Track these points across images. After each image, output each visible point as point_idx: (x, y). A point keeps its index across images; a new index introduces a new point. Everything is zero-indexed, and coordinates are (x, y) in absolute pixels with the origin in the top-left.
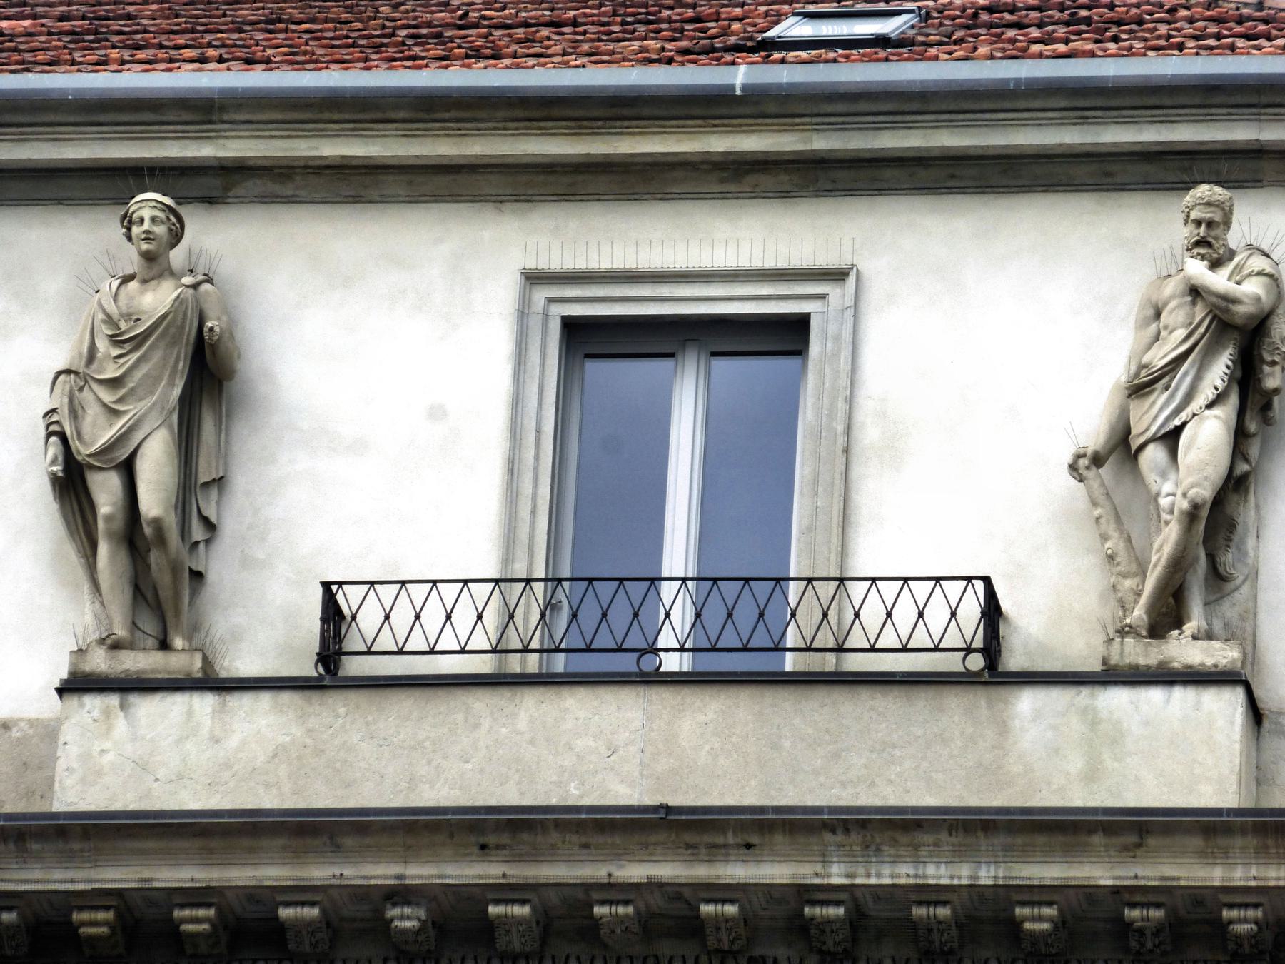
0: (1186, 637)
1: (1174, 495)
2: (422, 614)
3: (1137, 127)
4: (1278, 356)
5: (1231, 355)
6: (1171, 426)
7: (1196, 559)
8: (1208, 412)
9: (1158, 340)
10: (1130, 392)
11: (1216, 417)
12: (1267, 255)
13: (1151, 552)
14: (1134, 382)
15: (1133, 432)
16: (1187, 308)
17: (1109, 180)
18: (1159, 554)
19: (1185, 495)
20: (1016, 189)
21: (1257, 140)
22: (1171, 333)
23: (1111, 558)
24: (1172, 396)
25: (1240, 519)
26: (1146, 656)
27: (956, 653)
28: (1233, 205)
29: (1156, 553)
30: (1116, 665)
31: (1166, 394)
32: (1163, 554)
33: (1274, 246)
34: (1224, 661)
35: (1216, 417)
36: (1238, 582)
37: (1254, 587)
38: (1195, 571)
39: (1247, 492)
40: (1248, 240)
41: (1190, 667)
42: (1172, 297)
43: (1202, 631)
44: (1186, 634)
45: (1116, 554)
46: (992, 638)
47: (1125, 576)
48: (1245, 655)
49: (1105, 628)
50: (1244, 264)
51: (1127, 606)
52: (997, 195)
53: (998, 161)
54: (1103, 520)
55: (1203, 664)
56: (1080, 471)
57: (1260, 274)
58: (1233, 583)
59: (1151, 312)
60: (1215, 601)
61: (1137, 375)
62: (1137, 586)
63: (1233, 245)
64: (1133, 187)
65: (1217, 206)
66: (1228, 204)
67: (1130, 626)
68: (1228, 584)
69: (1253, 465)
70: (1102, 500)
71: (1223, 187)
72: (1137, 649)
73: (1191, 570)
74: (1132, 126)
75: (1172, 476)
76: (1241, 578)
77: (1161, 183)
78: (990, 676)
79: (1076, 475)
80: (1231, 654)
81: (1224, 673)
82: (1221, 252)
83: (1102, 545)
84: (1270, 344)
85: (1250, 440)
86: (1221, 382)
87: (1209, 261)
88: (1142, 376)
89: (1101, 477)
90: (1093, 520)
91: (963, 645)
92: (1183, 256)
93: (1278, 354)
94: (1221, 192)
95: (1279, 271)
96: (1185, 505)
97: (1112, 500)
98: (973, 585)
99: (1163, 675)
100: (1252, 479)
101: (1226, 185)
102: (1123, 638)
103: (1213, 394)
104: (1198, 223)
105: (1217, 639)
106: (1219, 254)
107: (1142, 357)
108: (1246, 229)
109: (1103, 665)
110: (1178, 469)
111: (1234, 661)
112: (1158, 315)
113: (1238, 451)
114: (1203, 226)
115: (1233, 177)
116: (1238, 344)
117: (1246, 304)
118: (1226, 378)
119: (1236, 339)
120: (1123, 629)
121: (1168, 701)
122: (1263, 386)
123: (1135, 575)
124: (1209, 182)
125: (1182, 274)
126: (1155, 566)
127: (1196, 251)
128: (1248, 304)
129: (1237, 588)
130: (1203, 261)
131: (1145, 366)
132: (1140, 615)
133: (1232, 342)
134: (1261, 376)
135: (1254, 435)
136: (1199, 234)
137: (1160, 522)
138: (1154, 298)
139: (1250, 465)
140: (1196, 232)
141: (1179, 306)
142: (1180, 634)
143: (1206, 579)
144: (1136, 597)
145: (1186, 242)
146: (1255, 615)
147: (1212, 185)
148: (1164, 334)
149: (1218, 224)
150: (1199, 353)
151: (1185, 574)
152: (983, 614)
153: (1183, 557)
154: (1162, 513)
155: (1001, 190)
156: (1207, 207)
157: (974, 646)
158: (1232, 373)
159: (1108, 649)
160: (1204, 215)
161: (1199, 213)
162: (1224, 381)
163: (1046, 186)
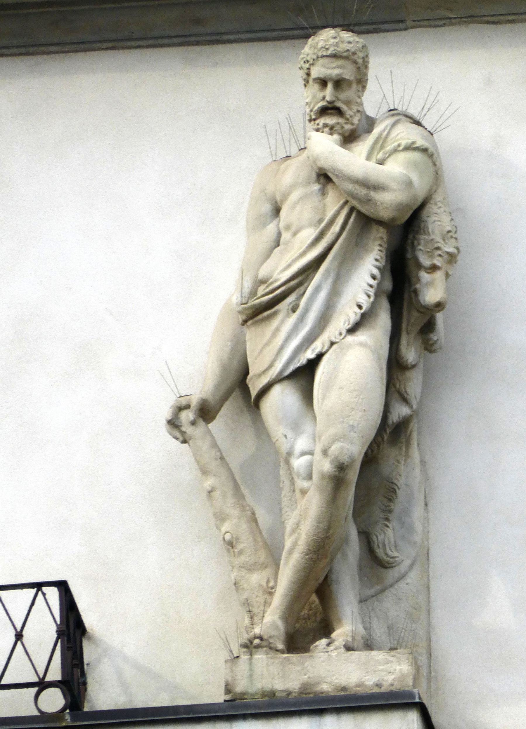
0: (336, 649)
1: (311, 453)
2: (24, 633)
4: (440, 259)
5: (377, 260)
7: (346, 540)
8: (350, 339)
9: (278, 245)
10: (244, 317)
11: (362, 345)
12: (418, 123)
13: (283, 534)
14: (251, 304)
16: (315, 200)
19: (325, 453)
20: (73, 47)
22: (295, 234)
23: (231, 544)
25: (401, 482)
27: (25, 690)
28: (367, 56)
29: (289, 538)
30: (243, 694)
31: (294, 317)
32: (300, 534)
33: (426, 109)
34: (391, 678)
35: (362, 345)
37: (426, 572)
38: (345, 554)
39: (408, 443)
40: (391, 103)
41: (344, 689)
42: (293, 187)
43: (358, 638)
44: (337, 643)
45: (237, 539)
46: (73, 666)
47: (251, 568)
48: (417, 668)
49: (227, 643)
50: (387, 137)
51: (255, 610)
52: (45, 57)
53: (45, 10)
54: (217, 494)
55: (361, 685)
57: (409, 148)
58: (396, 569)
59: (267, 208)
60: (373, 596)
61: (253, 293)
62: (268, 581)
63: (371, 112)
64: (232, 37)
65: (347, 58)
66: (361, 55)
67: (261, 638)
68: (391, 571)
69: (415, 407)
70: (214, 465)
71: (353, 32)
73: (339, 555)
75: (308, 428)
76: (407, 563)
77: (268, 31)
78: (73, 719)
79: (178, 435)
80: (398, 668)
82: (356, 121)
83: (218, 528)
84: (427, 242)
86: (366, 297)
87: (340, 134)
88: (259, 294)
89: (211, 435)
90: (205, 494)
91: (34, 679)
92: (305, 128)
93: (440, 255)
94: (351, 39)
95: (434, 145)
97: (227, 465)
98: (44, 594)
99: (308, 702)
100: (414, 426)
101: (356, 28)
102: (251, 654)
103: (356, 313)
104: (323, 83)
105: (379, 649)
106: (353, 124)
107: (258, 269)
108: (387, 88)
109: (225, 694)
110: (315, 418)
111: (403, 677)
112: (277, 211)
113: (393, 389)
114: (330, 86)
115: (365, 18)
116: (385, 246)
118: (372, 292)
119: (382, 238)
120: (251, 643)
122: (421, 299)
123: (263, 566)
124: (334, 27)
125: (306, 153)
126: (291, 552)
127: (322, 121)
128: (395, 190)
129: (402, 577)
130: (331, 134)
131: (263, 282)
132: (274, 622)
134: (417, 286)
135: (414, 366)
136: (324, 98)
137: (294, 491)
138: (270, 189)
139: (411, 407)
141: (304, 198)
142: (328, 645)
143: (360, 567)
144: (267, 596)
145: (308, 110)
146: (429, 612)
147: (338, 29)
148: (286, 236)
149: (349, 83)
150: (334, 259)
151: (332, 560)
152: (60, 634)
153: (327, 537)
154: (296, 479)
155: (52, 49)
156: (332, 60)
157: (48, 679)
158: (379, 284)
159: (232, 671)
161: (323, 70)
162: (369, 296)
163: (114, 41)
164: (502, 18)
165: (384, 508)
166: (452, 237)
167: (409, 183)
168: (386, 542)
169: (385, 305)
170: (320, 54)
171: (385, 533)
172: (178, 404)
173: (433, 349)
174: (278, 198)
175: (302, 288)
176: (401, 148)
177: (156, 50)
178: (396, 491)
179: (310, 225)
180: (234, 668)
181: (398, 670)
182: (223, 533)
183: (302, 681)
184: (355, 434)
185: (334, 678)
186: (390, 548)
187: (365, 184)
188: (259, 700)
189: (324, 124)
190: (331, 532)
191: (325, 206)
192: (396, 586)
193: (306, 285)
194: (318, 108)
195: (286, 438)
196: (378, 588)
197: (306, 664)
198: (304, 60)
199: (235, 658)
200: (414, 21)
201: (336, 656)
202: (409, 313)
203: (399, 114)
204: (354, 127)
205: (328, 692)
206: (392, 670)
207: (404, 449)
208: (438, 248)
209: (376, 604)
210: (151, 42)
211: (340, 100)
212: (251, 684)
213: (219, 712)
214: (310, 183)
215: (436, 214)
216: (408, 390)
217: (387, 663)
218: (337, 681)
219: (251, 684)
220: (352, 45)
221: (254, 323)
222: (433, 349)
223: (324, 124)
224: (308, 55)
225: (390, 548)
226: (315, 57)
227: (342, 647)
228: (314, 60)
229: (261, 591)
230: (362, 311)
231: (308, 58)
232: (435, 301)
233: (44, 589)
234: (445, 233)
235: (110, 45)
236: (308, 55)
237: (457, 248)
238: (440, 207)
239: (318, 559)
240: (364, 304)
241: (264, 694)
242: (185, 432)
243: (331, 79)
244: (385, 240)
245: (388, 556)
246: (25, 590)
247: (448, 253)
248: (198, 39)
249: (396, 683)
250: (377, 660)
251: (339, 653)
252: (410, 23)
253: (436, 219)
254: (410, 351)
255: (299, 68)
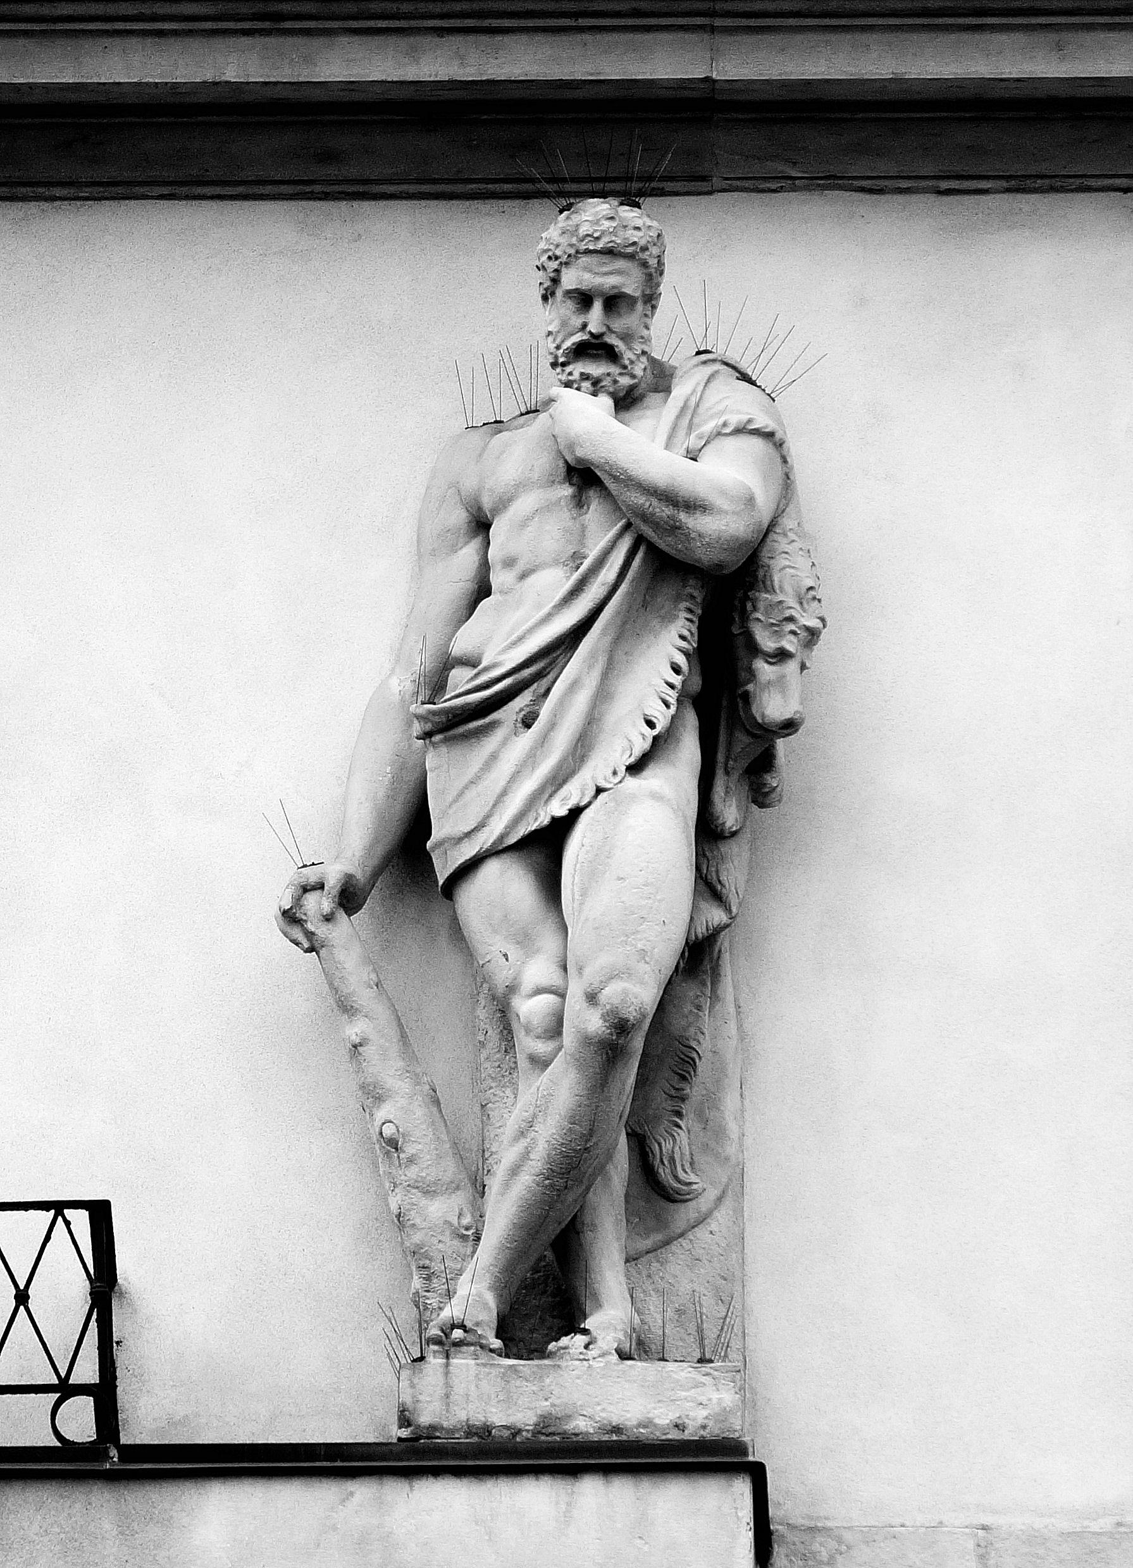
0: (603, 1355)
2: (30, 1292)
3: (403, 42)
4: (792, 637)
5: (683, 638)
6: (541, 818)
8: (632, 782)
11: (656, 797)
15: (437, 833)
17: (332, 171)
18: (523, 1143)
20: (96, 190)
21: (707, 79)
22: (523, 576)
24: (544, 740)
25: (704, 1046)
26: (508, 1401)
30: (433, 1428)
34: (701, 1415)
35: (656, 797)
36: (704, 1203)
37: (739, 1211)
38: (608, 1180)
41: (617, 1430)
42: (521, 486)
50: (697, 405)
52: (45, 205)
55: (647, 1424)
56: (310, 927)
59: (459, 517)
65: (631, 257)
66: (655, 251)
69: (734, 910)
72: (484, 1384)
74: (392, 40)
76: (712, 1194)
79: (300, 937)
80: (715, 1396)
81: (702, 1446)
82: (638, 371)
85: (725, 848)
90: (344, 1052)
93: (793, 633)
94: (639, 223)
96: (595, 1023)
98: (67, 1223)
100: (724, 941)
104: (584, 299)
106: (633, 376)
111: (723, 1415)
114: (597, 307)
117: (721, 511)
118: (672, 696)
121: (567, 1518)
124: (603, 195)
127: (578, 368)
130: (595, 394)
133: (684, 605)
134: (750, 687)
135: (734, 834)
138: (469, 484)
139: (728, 910)
140: (577, 321)
141: (547, 508)
150: (604, 632)
151: (588, 1189)
155: (58, 192)
156: (605, 259)
160: (598, 280)
161: (587, 276)
162: (667, 705)
164: (887, 183)
165: (673, 1092)
166: (814, 598)
167: (750, 501)
168: (677, 1157)
169: (691, 720)
170: (583, 247)
171: (674, 1140)
172: (303, 881)
173: (768, 802)
174: (487, 503)
175: (544, 683)
176: (728, 430)
177: (246, 204)
178: (695, 1063)
179: (556, 562)
180: (416, 1381)
181: (715, 1401)
182: (378, 1123)
183: (539, 1412)
184: (647, 966)
185: (599, 1408)
186: (683, 1165)
187: (669, 497)
188: (461, 1441)
189: (582, 374)
190: (594, 1140)
191: (583, 528)
192: (690, 1235)
193: (551, 677)
194: (573, 344)
195: (507, 960)
196: (658, 1237)
197: (548, 1381)
198: (550, 253)
199: (414, 1361)
200: (727, 179)
201: (603, 1368)
202: (730, 734)
203: (714, 361)
204: (636, 381)
205: (587, 1433)
206: (703, 1399)
207: (709, 984)
208: (791, 619)
209: (655, 1265)
210: (240, 189)
211: (614, 332)
212: (447, 1411)
213: (389, 1460)
214: (553, 482)
215: (786, 553)
216: (723, 878)
217: (696, 1387)
218: (604, 1415)
219: (447, 1411)
220: (640, 234)
221: (446, 740)
222: (768, 802)
223: (582, 374)
224: (557, 246)
225: (683, 1165)
226: (572, 251)
227: (614, 1351)
228: (569, 256)
229: (448, 1233)
230: (655, 732)
231: (558, 252)
232: (783, 718)
233: (68, 1212)
234: (804, 590)
235: (165, 190)
236: (557, 246)
237: (823, 620)
238: (793, 541)
239: (566, 1187)
240: (658, 719)
241: (471, 1430)
242: (313, 933)
243: (601, 294)
244: (699, 600)
245: (679, 1181)
246: (31, 1212)
247: (808, 629)
248: (328, 189)
249: (711, 1423)
250: (678, 1381)
251: (607, 1363)
252: (717, 182)
253: (787, 563)
254: (730, 806)
255: (537, 267)
